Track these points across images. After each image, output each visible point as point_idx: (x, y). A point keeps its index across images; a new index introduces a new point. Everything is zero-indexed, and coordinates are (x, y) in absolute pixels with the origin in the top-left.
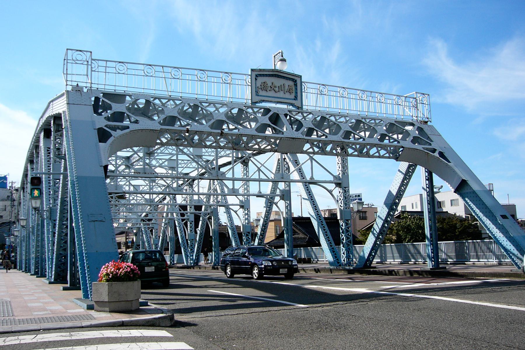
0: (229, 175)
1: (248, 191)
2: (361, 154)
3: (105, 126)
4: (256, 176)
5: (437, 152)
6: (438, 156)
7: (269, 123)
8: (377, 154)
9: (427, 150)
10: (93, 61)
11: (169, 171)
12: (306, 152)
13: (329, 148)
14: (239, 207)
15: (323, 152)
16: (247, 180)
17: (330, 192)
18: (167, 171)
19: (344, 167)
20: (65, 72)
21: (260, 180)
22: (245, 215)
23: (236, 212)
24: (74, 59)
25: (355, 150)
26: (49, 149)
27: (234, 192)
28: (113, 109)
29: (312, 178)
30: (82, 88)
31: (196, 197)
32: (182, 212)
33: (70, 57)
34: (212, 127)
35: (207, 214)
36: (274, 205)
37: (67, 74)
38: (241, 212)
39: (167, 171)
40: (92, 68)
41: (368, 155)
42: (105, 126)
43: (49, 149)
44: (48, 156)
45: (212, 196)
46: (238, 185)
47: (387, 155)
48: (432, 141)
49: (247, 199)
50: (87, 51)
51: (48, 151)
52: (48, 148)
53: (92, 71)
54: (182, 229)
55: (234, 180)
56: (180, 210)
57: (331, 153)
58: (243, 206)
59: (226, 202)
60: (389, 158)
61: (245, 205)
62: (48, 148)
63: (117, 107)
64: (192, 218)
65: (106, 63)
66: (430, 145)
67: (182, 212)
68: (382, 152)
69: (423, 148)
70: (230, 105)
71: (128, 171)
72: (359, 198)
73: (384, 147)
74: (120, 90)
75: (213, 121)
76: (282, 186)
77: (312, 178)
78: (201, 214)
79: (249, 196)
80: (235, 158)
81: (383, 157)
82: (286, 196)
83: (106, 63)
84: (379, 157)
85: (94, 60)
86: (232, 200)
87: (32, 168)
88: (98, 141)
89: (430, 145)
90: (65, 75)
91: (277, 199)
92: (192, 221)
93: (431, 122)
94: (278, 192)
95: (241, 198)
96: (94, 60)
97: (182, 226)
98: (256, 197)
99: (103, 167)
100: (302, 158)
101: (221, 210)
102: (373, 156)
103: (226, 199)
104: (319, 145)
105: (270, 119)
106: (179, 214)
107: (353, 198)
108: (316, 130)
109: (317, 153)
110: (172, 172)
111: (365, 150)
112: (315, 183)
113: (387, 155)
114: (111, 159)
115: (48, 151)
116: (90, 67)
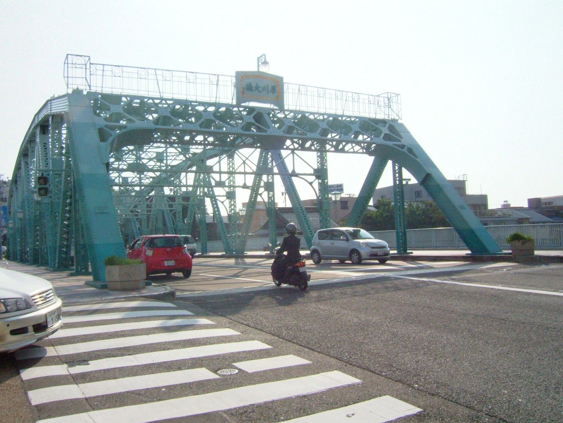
0: (216, 168)
1: (234, 183)
2: (337, 150)
3: (105, 126)
4: (241, 169)
5: (406, 148)
6: (406, 151)
7: (253, 121)
8: (352, 150)
9: (398, 146)
10: (91, 65)
11: (155, 164)
12: (288, 148)
13: (308, 145)
14: (225, 198)
15: (303, 148)
16: (231, 173)
17: (311, 184)
18: (156, 164)
19: (322, 160)
20: (66, 75)
21: (245, 173)
22: (231, 205)
23: (222, 202)
24: (74, 63)
25: (332, 146)
26: (45, 145)
27: (220, 184)
28: (111, 110)
29: (293, 171)
30: (82, 91)
31: (184, 189)
32: (171, 203)
33: (70, 62)
34: (201, 126)
35: (195, 205)
36: (259, 196)
37: (68, 77)
38: (227, 202)
39: (156, 164)
40: (90, 72)
41: (343, 151)
42: (105, 126)
43: (45, 145)
44: (45, 151)
45: (199, 188)
46: (224, 177)
47: (361, 151)
48: (402, 138)
49: (233, 190)
50: (85, 56)
51: (44, 146)
52: (44, 144)
53: (90, 74)
54: (171, 220)
55: (220, 173)
56: (168, 201)
57: (309, 149)
58: (229, 197)
59: (213, 194)
60: (363, 153)
61: (231, 196)
62: (44, 144)
63: (115, 109)
64: (180, 209)
65: (103, 67)
66: (400, 141)
67: (171, 203)
68: (357, 148)
69: (394, 144)
70: (217, 105)
71: (117, 163)
72: (340, 188)
73: (358, 143)
74: (116, 92)
75: (202, 120)
76: (265, 178)
77: (293, 171)
78: (188, 205)
79: (235, 187)
80: (221, 151)
81: (357, 152)
82: (270, 187)
83: (103, 67)
84: (354, 152)
85: (92, 64)
86: (219, 191)
87: (26, 162)
88: (99, 141)
89: (400, 141)
90: (66, 79)
91: (261, 190)
92: (180, 212)
93: (401, 119)
94: (262, 184)
95: (227, 189)
96: (92, 64)
97: (170, 217)
98: (241, 188)
99: (105, 165)
100: (284, 153)
101: (208, 201)
102: (348, 152)
103: (213, 191)
104: (299, 142)
105: (254, 118)
106: (167, 206)
107: (335, 188)
108: (296, 128)
109: (297, 149)
110: (160, 164)
111: (341, 146)
112: (297, 175)
113: (361, 151)
114: (156, 173)
115: (44, 146)
116: (88, 71)
